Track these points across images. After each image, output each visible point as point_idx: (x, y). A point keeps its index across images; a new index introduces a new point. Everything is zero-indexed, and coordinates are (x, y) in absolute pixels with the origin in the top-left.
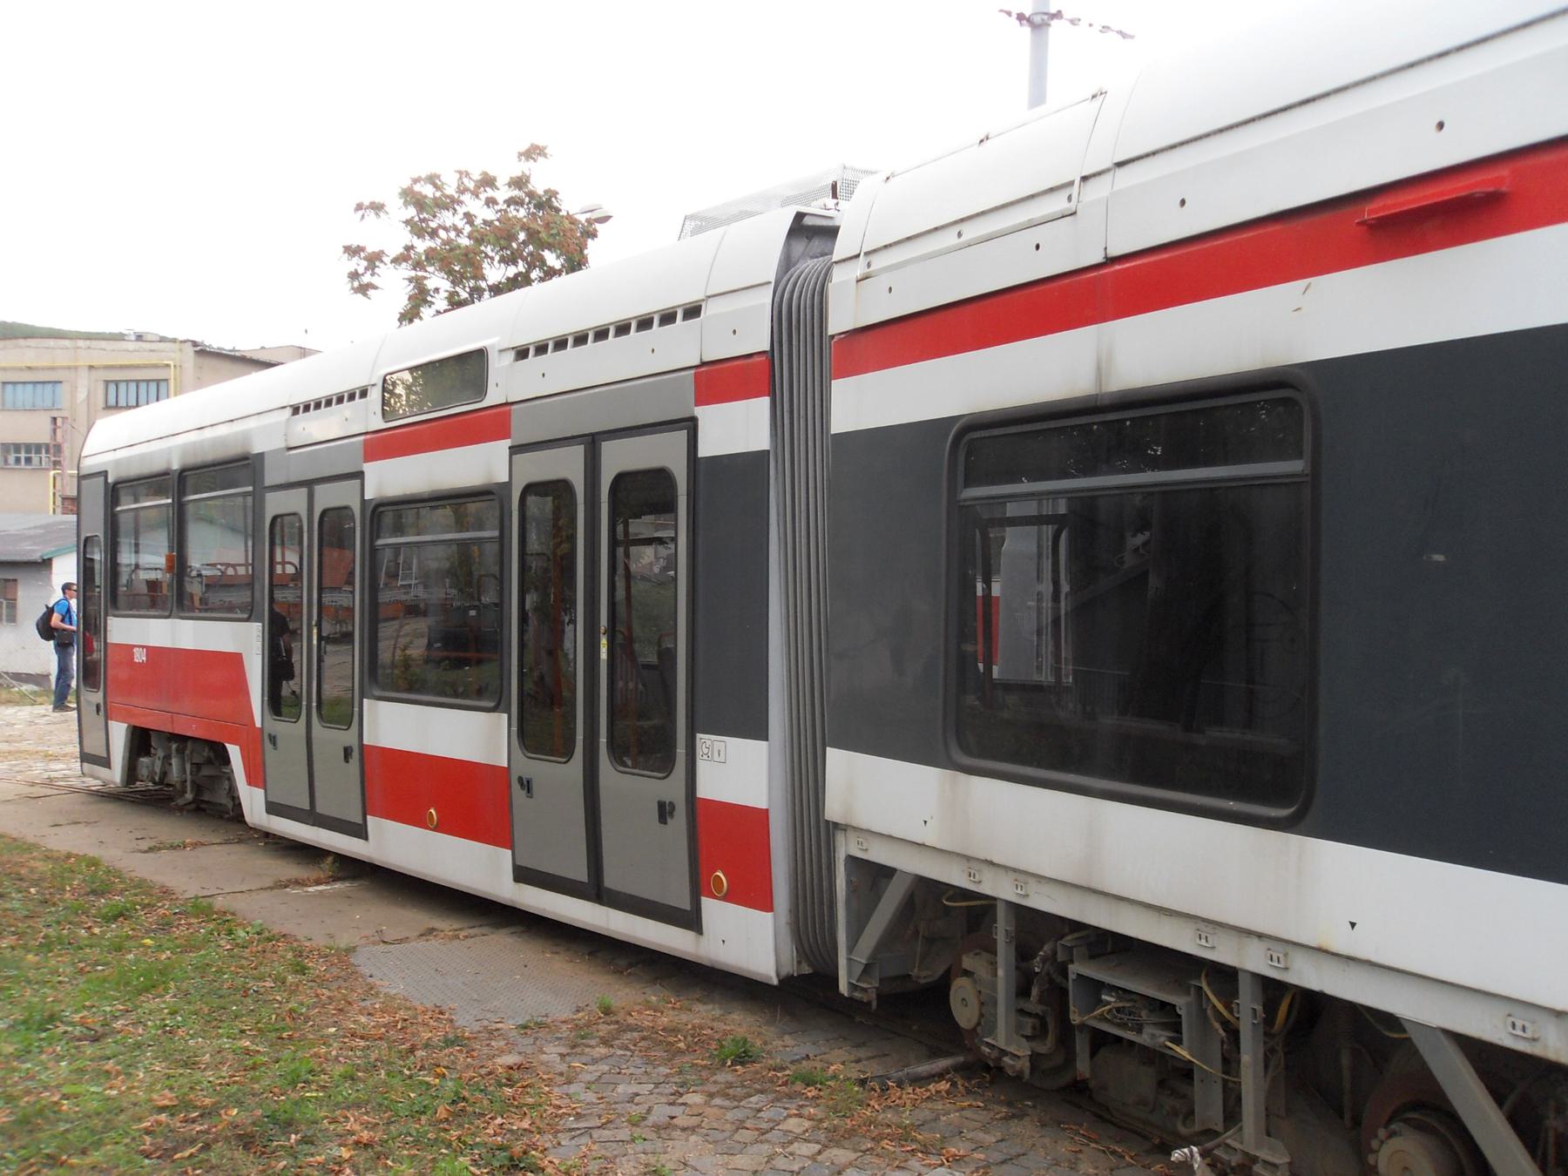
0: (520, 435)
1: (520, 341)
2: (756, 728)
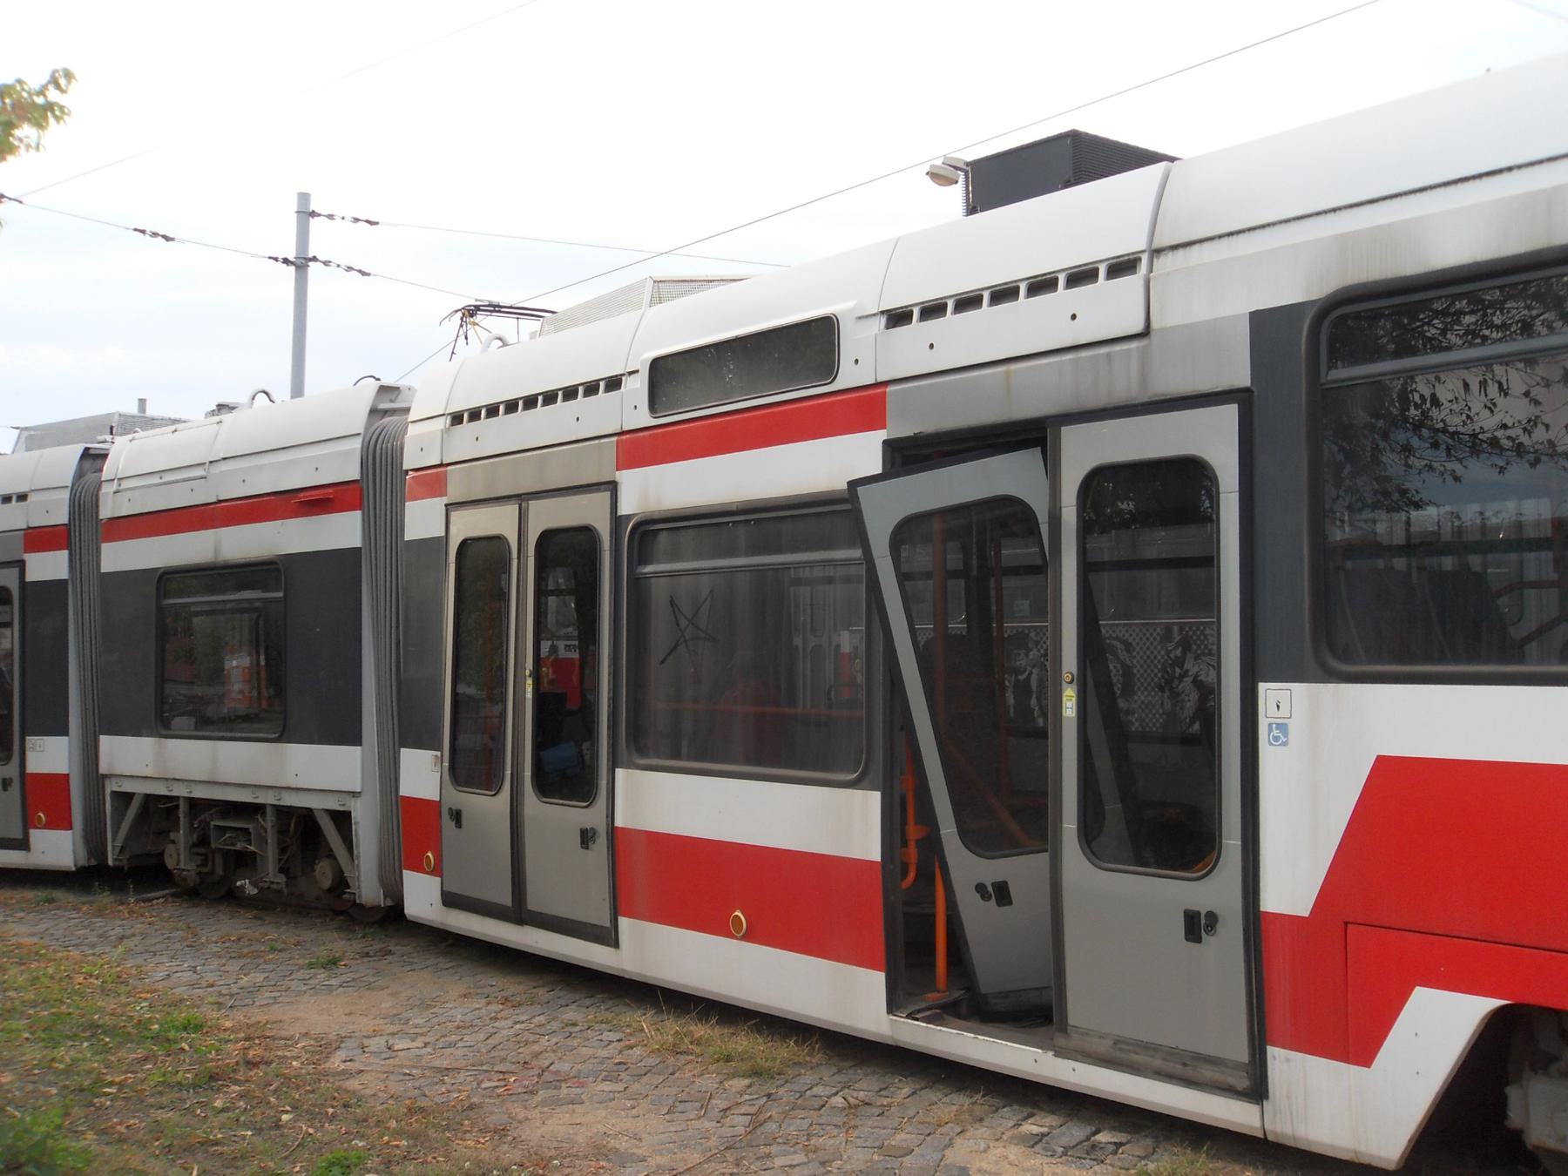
0: (455, 491)
1: (895, 302)
2: (62, 730)
